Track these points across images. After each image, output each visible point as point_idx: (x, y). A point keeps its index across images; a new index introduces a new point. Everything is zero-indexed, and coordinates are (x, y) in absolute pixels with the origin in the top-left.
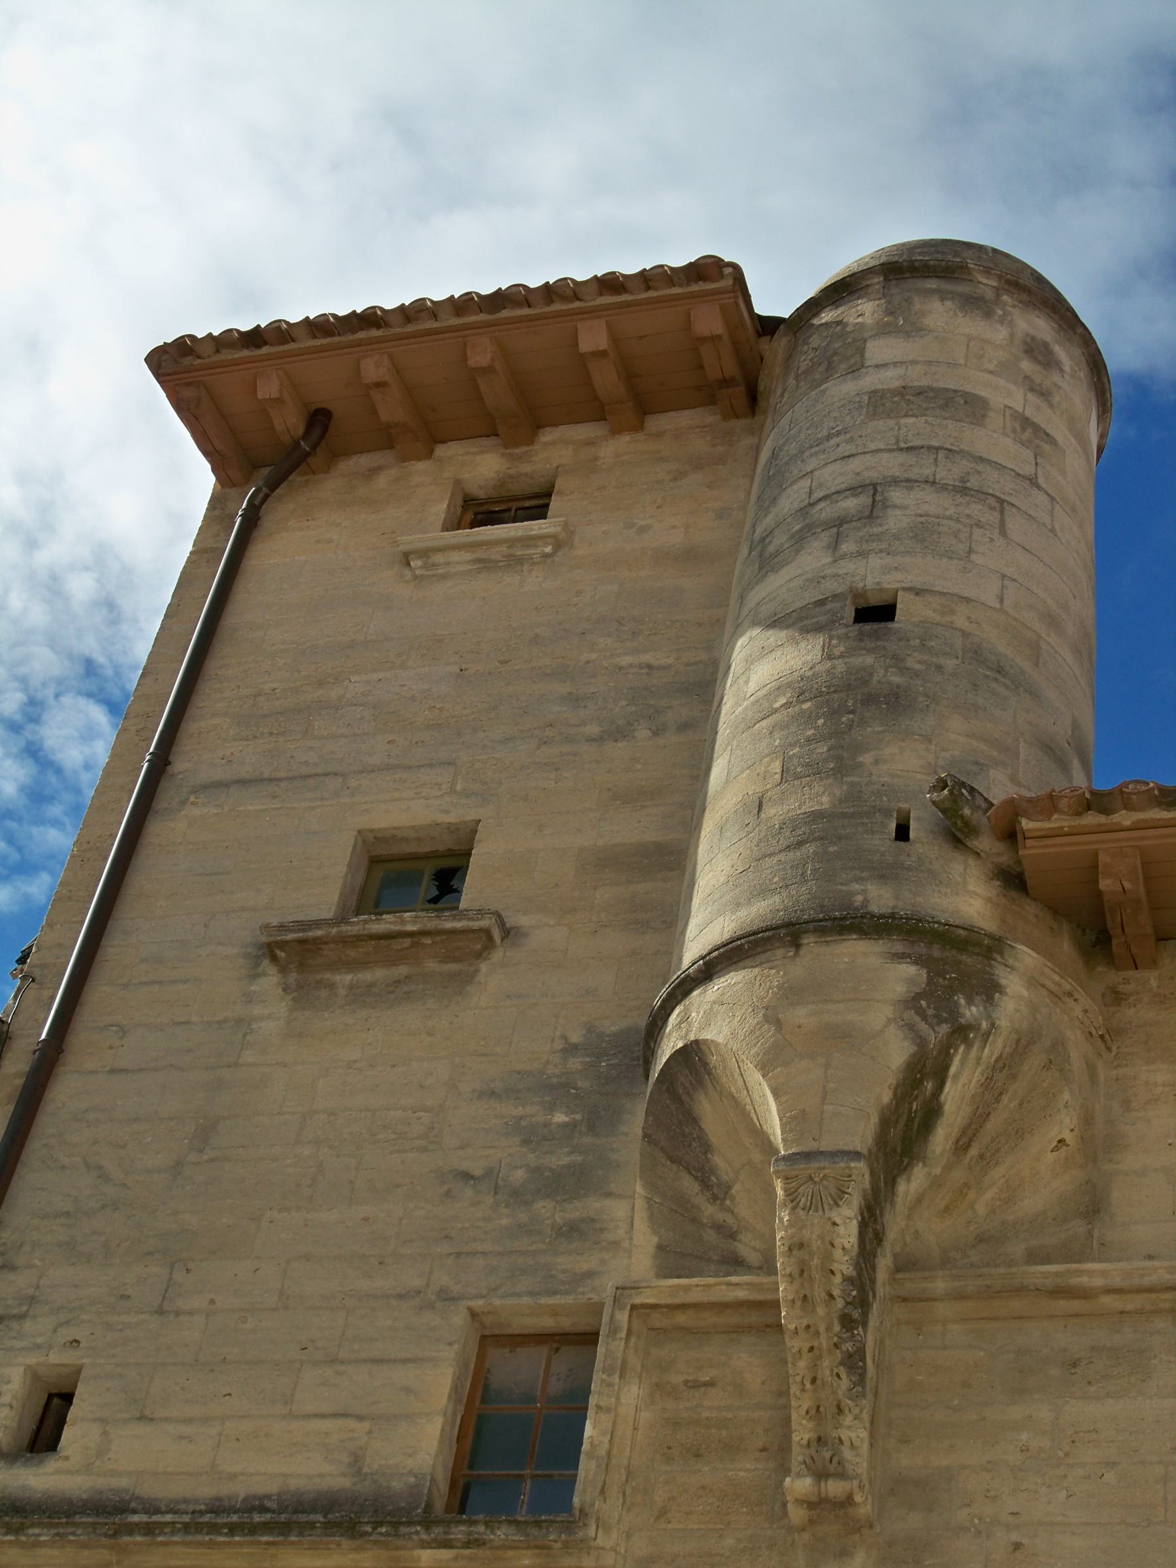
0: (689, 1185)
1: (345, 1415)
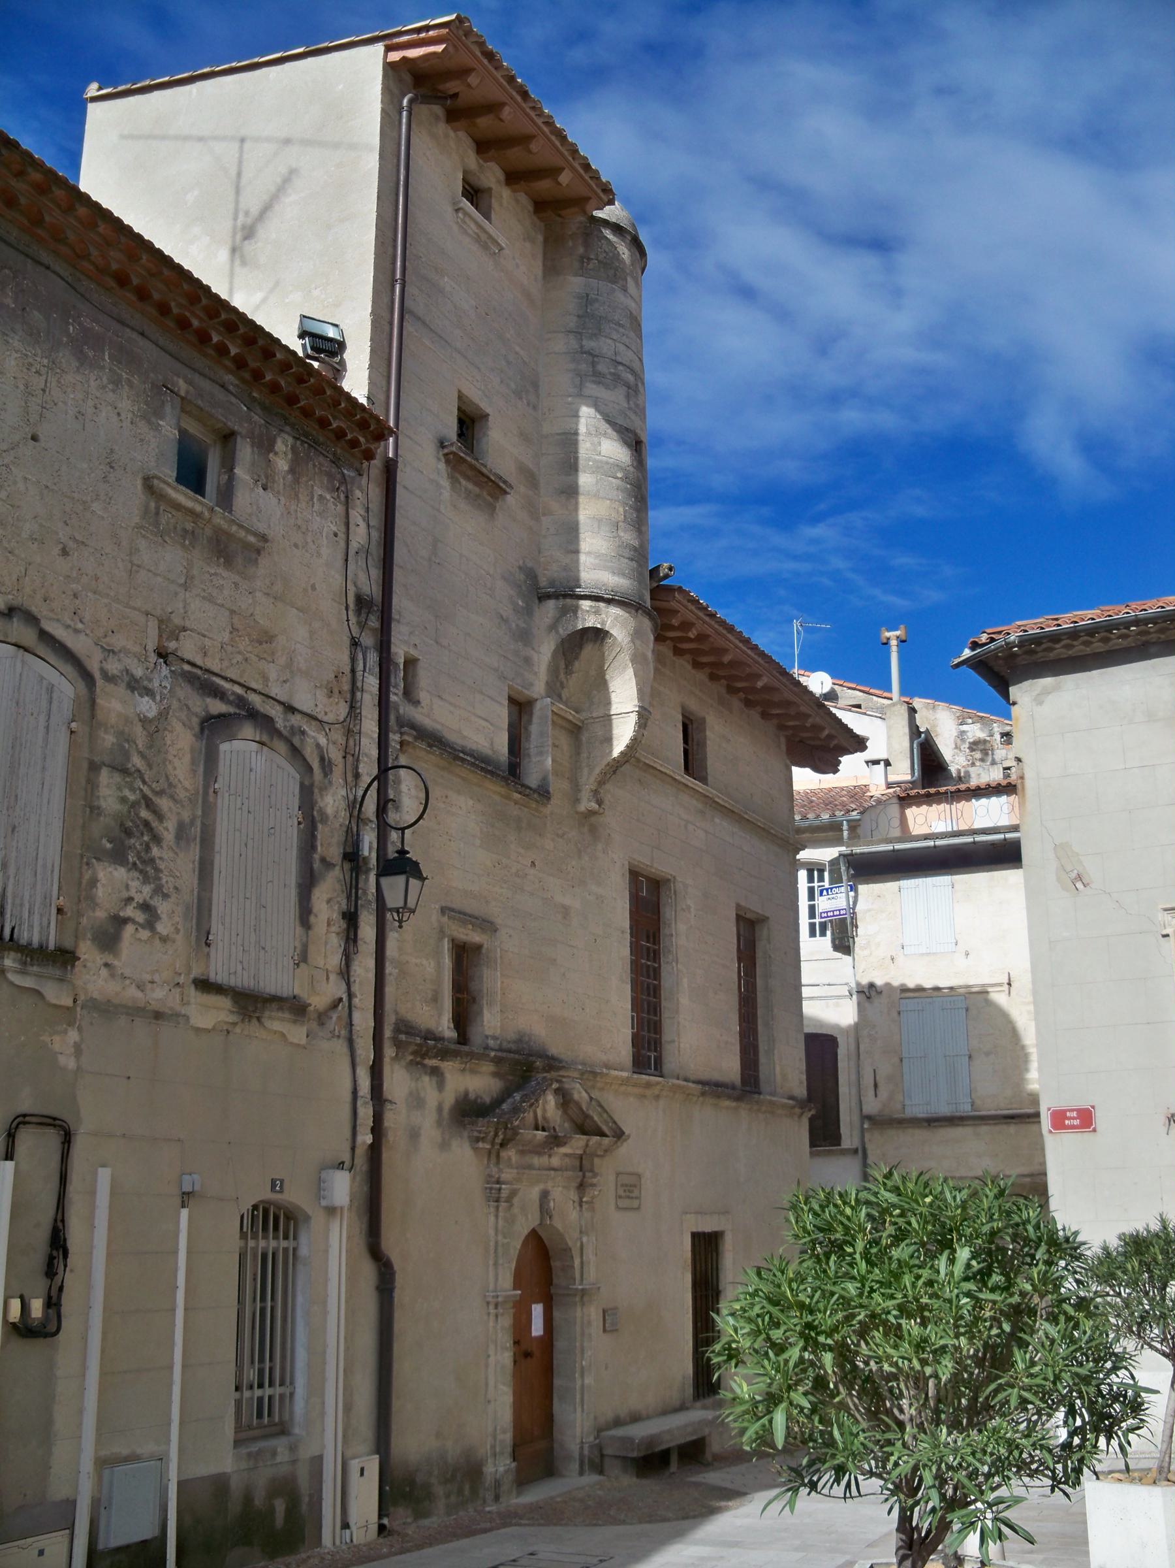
0: (562, 665)
1: (487, 720)
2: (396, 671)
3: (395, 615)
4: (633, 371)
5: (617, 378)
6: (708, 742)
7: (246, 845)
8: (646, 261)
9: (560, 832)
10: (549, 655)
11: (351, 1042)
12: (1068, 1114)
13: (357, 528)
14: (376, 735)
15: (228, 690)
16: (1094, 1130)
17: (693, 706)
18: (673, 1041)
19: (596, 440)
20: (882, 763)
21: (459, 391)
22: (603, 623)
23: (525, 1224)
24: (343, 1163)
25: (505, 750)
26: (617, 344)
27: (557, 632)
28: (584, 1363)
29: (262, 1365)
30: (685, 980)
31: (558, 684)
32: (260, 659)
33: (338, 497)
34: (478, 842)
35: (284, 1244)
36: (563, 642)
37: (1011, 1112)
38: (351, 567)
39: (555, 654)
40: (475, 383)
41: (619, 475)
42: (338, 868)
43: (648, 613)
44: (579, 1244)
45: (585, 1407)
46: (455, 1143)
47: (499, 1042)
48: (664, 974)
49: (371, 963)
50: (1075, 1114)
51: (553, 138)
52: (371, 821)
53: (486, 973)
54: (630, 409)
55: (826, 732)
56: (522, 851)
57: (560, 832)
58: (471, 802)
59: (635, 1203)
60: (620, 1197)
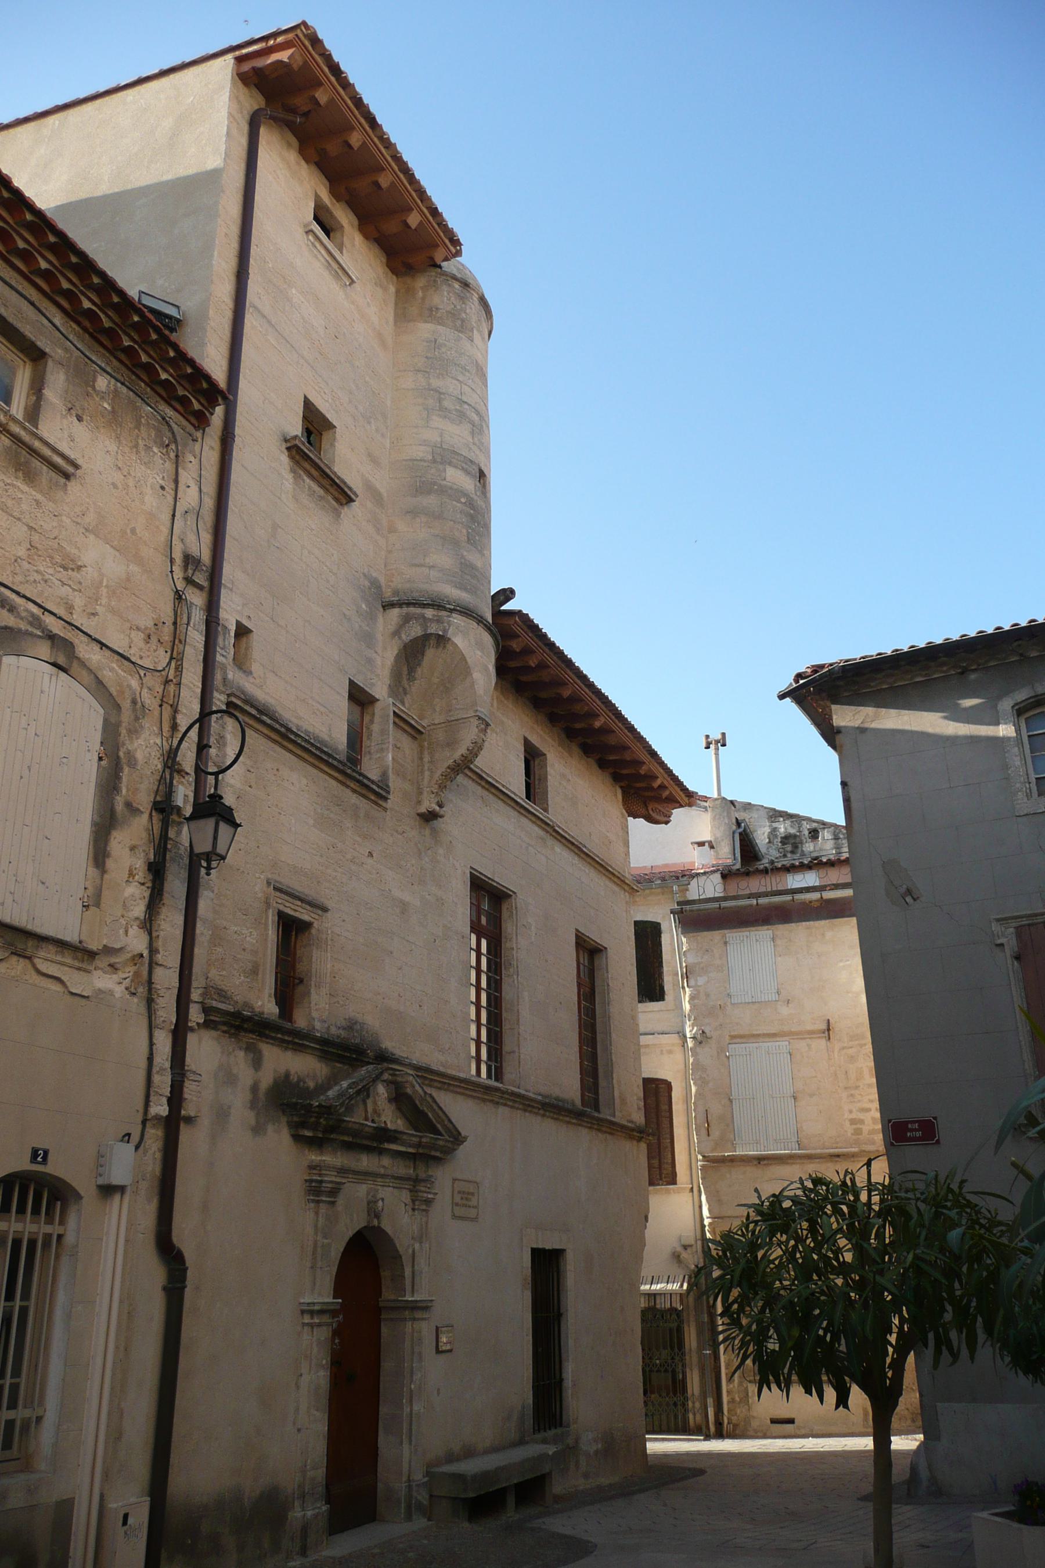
0: (405, 669)
2: (224, 634)
3: (224, 580)
4: (478, 413)
5: (462, 415)
6: (549, 777)
7: (29, 768)
8: (492, 324)
9: (400, 829)
10: (392, 659)
11: (150, 1002)
12: (910, 1126)
13: (188, 489)
14: (199, 691)
15: (21, 606)
16: (938, 1142)
17: (535, 740)
18: (514, 1052)
19: (441, 467)
20: (707, 844)
21: (305, 397)
22: (445, 631)
23: (349, 1224)
24: (129, 1135)
25: (344, 739)
26: (463, 386)
27: (400, 638)
28: (413, 1386)
29: (17, 1380)
30: (526, 994)
31: (401, 690)
32: (64, 584)
33: (168, 453)
34: (311, 822)
35: (48, 1229)
36: (405, 647)
37: (836, 1151)
38: (179, 523)
39: (397, 658)
40: (323, 394)
41: (463, 500)
42: (145, 817)
43: (488, 628)
44: (410, 1251)
45: (413, 1438)
46: (270, 1128)
47: (326, 1025)
48: (504, 986)
49: (180, 920)
50: (916, 1126)
51: (401, 176)
52: (187, 774)
53: (316, 954)
54: (474, 444)
55: (658, 782)
56: (358, 839)
57: (400, 829)
58: (304, 781)
59: (472, 1213)
60: (457, 1205)
